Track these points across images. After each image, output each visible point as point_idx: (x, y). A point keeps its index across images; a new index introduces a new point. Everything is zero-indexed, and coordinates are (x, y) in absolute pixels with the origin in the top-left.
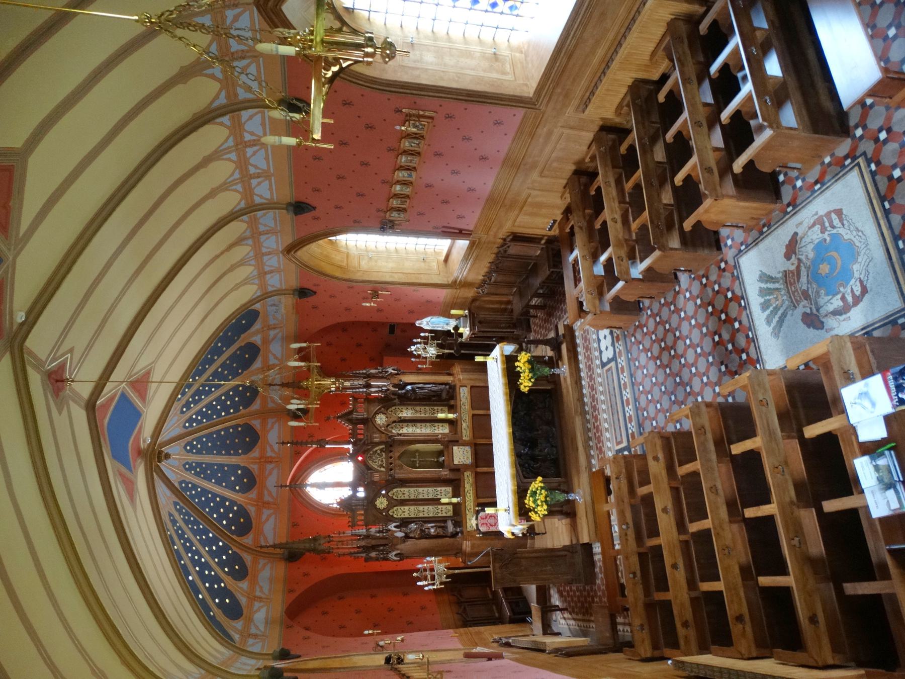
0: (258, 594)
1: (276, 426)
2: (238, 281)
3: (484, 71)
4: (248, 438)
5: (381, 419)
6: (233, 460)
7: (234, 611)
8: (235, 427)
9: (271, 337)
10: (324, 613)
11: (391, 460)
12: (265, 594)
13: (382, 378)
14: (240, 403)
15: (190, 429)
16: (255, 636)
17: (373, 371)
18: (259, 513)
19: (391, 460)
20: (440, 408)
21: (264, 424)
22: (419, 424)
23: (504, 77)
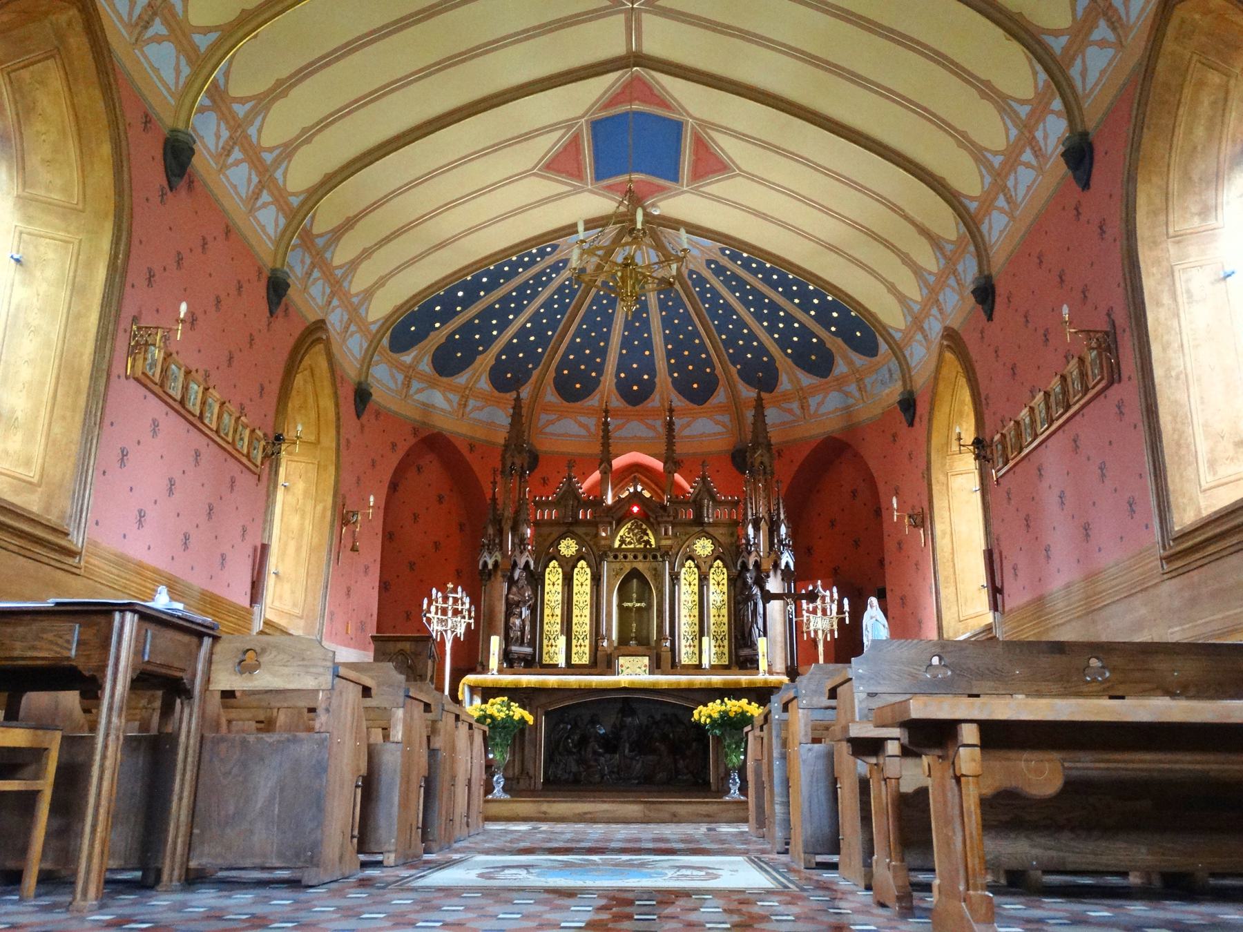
0: (471, 403)
1: (719, 429)
2: (900, 288)
3: (1206, 425)
4: (697, 387)
5: (703, 547)
6: (661, 364)
7: (448, 362)
8: (709, 362)
9: (846, 389)
10: (440, 499)
11: (631, 557)
12: (466, 408)
13: (771, 544)
14: (746, 363)
15: (690, 283)
16: (408, 386)
17: (783, 530)
18: (590, 412)
19: (631, 557)
20: (726, 650)
21: (722, 409)
22: (696, 612)
23: (1203, 468)
